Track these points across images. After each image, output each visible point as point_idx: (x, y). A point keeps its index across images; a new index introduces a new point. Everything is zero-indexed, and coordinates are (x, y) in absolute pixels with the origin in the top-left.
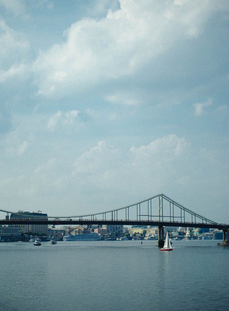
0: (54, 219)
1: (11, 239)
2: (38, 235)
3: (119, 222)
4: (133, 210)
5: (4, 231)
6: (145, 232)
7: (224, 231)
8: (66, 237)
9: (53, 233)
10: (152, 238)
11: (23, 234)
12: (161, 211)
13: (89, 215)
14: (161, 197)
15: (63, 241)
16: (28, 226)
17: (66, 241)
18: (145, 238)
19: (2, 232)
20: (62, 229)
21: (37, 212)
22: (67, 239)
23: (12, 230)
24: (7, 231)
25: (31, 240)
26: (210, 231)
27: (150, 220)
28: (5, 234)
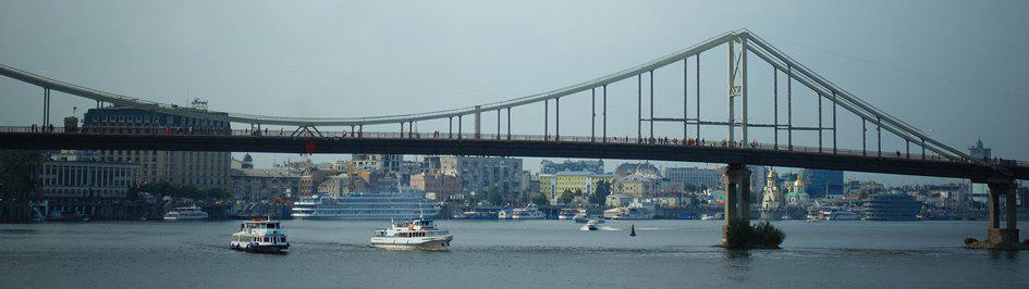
0: (295, 128)
1: (89, 208)
2: (194, 194)
3: (466, 141)
4: (623, 96)
5: (60, 175)
6: (603, 190)
7: (997, 191)
8: (302, 203)
9: (249, 188)
10: (633, 210)
11: (134, 192)
12: (738, 101)
13: (442, 116)
14: (738, 48)
15: (293, 218)
16: (205, 155)
17: (304, 218)
18: (607, 213)
19: (54, 183)
20: (286, 174)
21: (190, 106)
22: (307, 212)
23: (93, 176)
24: (73, 176)
25: (171, 215)
26: (845, 190)
27: (455, 131)
28: (76, 189)
